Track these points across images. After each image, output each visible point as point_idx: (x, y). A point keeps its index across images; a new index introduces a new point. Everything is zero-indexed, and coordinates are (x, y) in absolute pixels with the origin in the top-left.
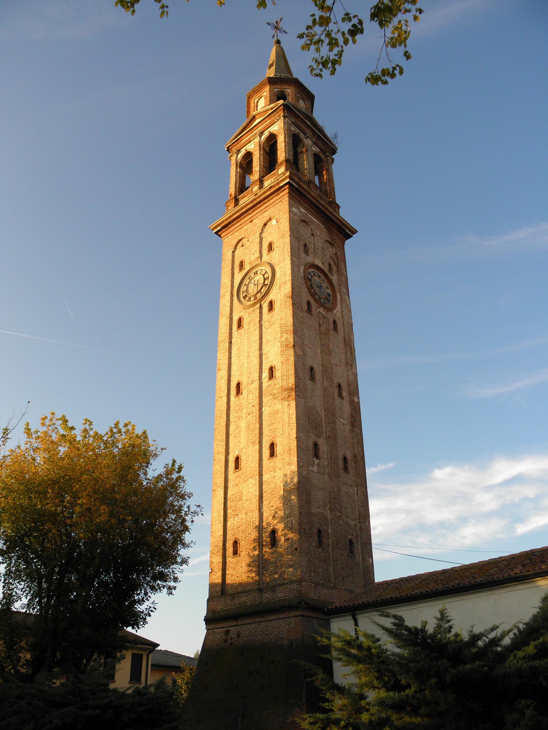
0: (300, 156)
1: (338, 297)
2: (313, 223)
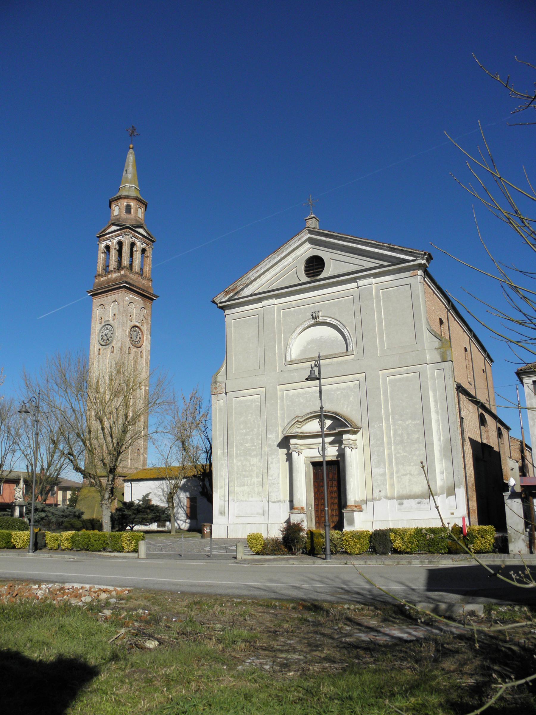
1: (145, 338)
2: (135, 300)
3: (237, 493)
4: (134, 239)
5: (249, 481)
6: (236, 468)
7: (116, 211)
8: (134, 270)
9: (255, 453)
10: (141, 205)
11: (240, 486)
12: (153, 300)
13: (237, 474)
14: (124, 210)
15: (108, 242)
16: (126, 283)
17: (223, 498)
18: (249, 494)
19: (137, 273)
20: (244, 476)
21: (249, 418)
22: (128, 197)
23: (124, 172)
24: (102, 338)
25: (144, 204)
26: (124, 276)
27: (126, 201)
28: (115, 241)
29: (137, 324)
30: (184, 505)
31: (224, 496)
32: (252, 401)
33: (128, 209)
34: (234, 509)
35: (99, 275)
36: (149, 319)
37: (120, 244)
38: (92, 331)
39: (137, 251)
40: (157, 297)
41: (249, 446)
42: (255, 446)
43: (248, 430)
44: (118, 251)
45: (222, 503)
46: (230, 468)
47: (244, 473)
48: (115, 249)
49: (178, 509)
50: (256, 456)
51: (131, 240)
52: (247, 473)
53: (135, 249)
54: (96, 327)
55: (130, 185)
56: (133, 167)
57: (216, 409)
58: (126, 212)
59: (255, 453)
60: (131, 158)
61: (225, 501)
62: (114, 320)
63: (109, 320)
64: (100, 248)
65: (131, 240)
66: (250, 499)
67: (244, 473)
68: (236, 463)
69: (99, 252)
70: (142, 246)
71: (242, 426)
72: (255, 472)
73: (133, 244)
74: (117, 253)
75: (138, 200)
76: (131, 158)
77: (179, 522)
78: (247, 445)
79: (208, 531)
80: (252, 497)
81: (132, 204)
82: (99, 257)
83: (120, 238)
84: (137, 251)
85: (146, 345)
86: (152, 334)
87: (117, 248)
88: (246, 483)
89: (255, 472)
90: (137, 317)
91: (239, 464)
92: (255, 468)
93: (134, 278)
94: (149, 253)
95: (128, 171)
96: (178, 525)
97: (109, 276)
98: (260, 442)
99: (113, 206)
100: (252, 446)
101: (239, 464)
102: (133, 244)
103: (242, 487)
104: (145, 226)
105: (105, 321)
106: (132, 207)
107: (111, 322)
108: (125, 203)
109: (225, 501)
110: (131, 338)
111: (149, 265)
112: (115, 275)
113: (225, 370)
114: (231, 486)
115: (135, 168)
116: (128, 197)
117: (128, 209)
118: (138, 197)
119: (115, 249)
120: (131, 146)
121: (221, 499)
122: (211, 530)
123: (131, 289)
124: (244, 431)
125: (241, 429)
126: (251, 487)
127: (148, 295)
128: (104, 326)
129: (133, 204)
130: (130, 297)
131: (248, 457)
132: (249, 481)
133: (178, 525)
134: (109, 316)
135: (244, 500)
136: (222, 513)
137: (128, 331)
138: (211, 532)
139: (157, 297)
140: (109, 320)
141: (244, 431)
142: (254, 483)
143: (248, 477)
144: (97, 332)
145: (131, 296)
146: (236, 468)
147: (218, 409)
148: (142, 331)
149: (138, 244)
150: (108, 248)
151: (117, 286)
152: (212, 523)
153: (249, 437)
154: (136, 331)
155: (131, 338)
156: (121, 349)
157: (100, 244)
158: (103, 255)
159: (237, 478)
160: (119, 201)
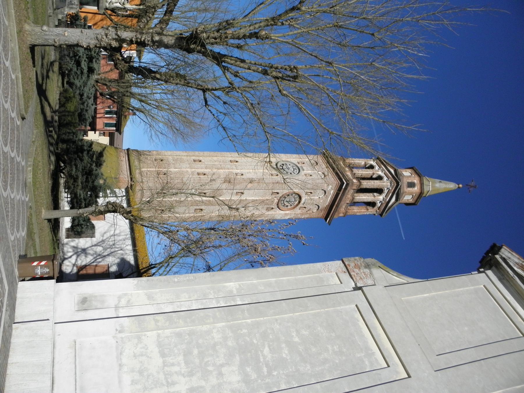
0: (371, 194)
1: (287, 212)
2: (327, 197)
3: (139, 338)
4: (386, 191)
5: (176, 369)
6: (205, 328)
7: (406, 173)
8: (356, 195)
9: (254, 376)
10: (415, 198)
11: (160, 345)
12: (326, 219)
13: (191, 333)
14: (410, 181)
15: (377, 168)
16: (347, 185)
17: (123, 302)
18: (141, 372)
19: (353, 199)
20: (187, 354)
21: (330, 347)
22: (422, 184)
23: (439, 180)
24: (283, 164)
25: (416, 201)
26: (353, 182)
27: (418, 182)
28: (380, 173)
29: (302, 202)
30: (100, 262)
31: (129, 304)
32: (367, 348)
33: (411, 185)
34: (98, 335)
35: (344, 160)
36: (307, 216)
37: (380, 178)
38: (288, 155)
39: (374, 196)
40: (329, 223)
41: (264, 357)
42: (270, 373)
43: (301, 348)
44: (372, 176)
45: (112, 302)
46: (202, 313)
47: (196, 352)
48: (374, 174)
49: (92, 255)
50: (246, 380)
51: (386, 189)
52: (197, 361)
53: (375, 194)
54: (293, 159)
55: (436, 186)
56: (445, 188)
57: (320, 272)
58: (408, 183)
59: (254, 376)
60: (452, 186)
61: (117, 308)
62: (306, 175)
63: (304, 170)
64: (369, 160)
65: (386, 189)
66: (127, 379)
67: (196, 352)
68: (216, 329)
69: (366, 160)
70: (378, 202)
71: (305, 333)
72: (203, 383)
73: (379, 191)
74: (369, 177)
75: (421, 193)
76: (452, 186)
77: (74, 257)
78: (266, 350)
79: (39, 272)
80: (134, 382)
81: (416, 188)
82: (361, 160)
83: (385, 178)
84: (374, 196)
85: (279, 214)
86: (289, 222)
87: (374, 176)
88: (169, 360)
89: (203, 383)
90: (309, 201)
91: (217, 336)
92: (213, 380)
93: (349, 195)
94: (371, 211)
95: (441, 184)
96: (71, 257)
97: (347, 169)
98: (283, 387)
99: (410, 171)
100: (267, 365)
101: (217, 336)
102: (379, 191)
103: (157, 350)
104: (397, 203)
105: (302, 167)
106: (414, 189)
107: (302, 173)
108: (416, 181)
109: (117, 308)
110: (288, 195)
111: (360, 212)
112: (349, 174)
113: (394, 282)
114: (157, 321)
115: (444, 191)
116: (422, 184)
117: (411, 185)
118: (423, 193)
119: (374, 174)
120: (461, 186)
121: (120, 298)
122: (41, 278)
123: (340, 191)
124: (296, 339)
125: (298, 331)
126: (162, 376)
127: (332, 212)
128: (297, 166)
129: (416, 189)
130: (332, 192)
131: (238, 358)
132: (176, 369)
133: (71, 257)
134: (308, 170)
135: (124, 361)
136: (84, 303)
137: (296, 191)
138: (34, 279)
139: (329, 223)
140: (304, 170)
141: (296, 339)
142: (173, 384)
143: (187, 363)
144: (289, 160)
145: (332, 192)
146: (205, 328)
147: (321, 275)
148: (294, 208)
149: (381, 197)
150: (372, 167)
151: (341, 176)
152: (57, 281)
153: (285, 353)
154: (295, 201)
155: (288, 195)
156: (277, 183)
157: (372, 160)
158: (363, 163)
159: (179, 335)
160: (416, 176)
